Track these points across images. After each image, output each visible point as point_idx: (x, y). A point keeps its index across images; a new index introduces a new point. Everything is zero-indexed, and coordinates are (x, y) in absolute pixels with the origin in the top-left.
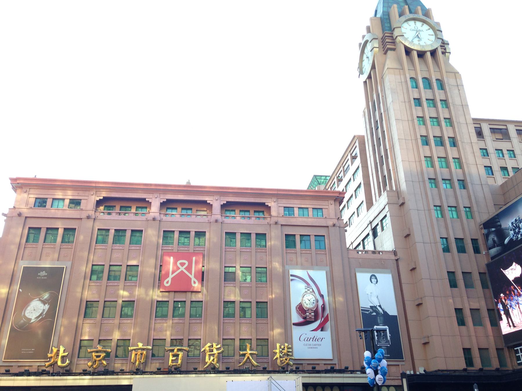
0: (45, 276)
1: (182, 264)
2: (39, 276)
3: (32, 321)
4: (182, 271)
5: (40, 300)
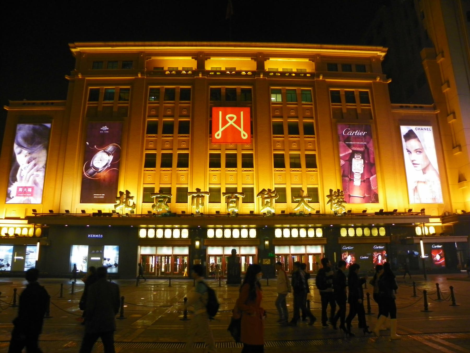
0: (107, 130)
1: (231, 118)
2: (102, 130)
3: (100, 170)
4: (228, 122)
5: (105, 152)
